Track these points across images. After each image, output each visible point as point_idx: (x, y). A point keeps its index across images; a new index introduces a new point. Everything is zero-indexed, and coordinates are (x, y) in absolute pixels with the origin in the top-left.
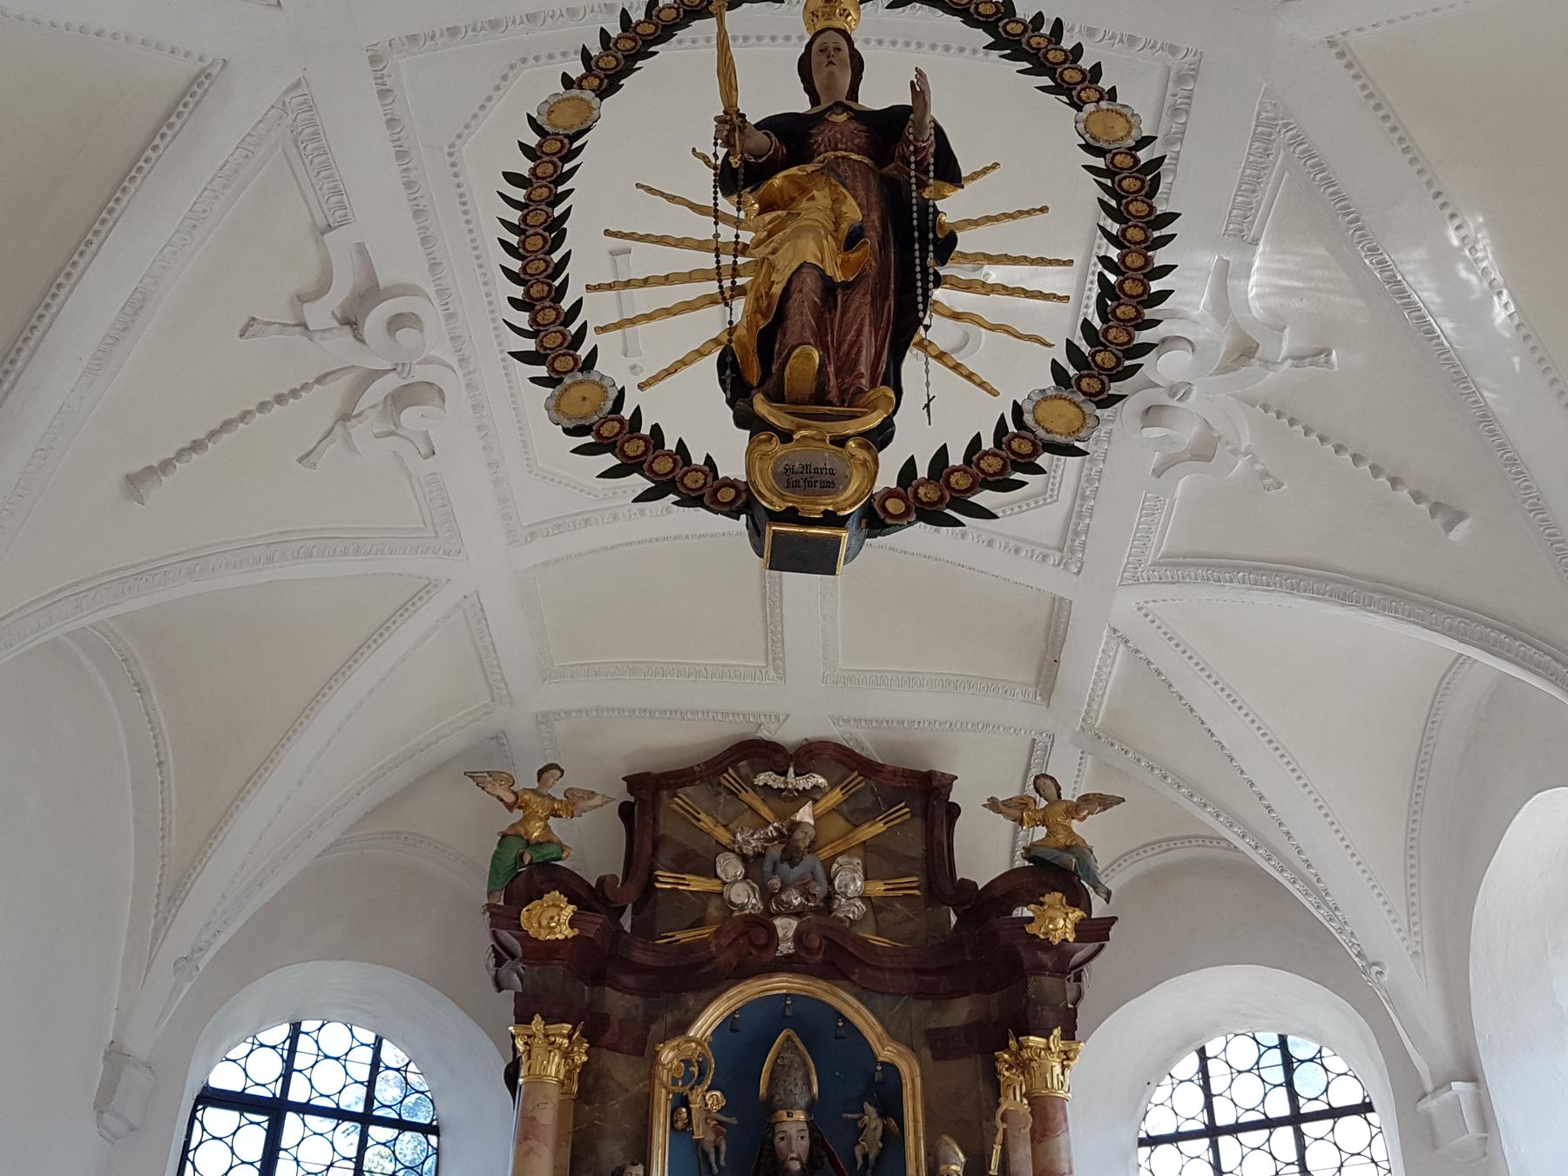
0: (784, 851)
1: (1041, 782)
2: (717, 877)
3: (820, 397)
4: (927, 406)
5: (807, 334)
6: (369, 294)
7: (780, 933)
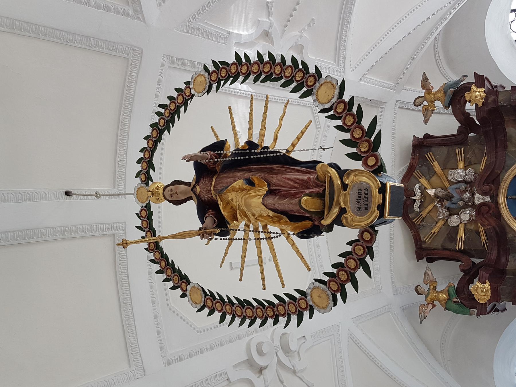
0: (447, 200)
1: (417, 104)
2: (458, 226)
3: (321, 196)
4: (324, 149)
5: (294, 201)
6: (250, 363)
7: (481, 201)
